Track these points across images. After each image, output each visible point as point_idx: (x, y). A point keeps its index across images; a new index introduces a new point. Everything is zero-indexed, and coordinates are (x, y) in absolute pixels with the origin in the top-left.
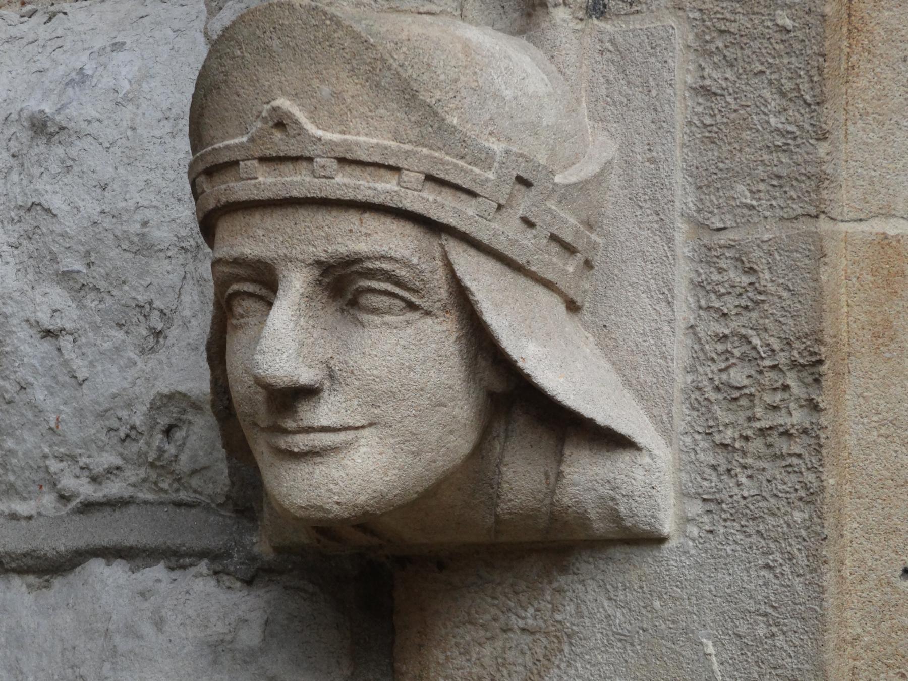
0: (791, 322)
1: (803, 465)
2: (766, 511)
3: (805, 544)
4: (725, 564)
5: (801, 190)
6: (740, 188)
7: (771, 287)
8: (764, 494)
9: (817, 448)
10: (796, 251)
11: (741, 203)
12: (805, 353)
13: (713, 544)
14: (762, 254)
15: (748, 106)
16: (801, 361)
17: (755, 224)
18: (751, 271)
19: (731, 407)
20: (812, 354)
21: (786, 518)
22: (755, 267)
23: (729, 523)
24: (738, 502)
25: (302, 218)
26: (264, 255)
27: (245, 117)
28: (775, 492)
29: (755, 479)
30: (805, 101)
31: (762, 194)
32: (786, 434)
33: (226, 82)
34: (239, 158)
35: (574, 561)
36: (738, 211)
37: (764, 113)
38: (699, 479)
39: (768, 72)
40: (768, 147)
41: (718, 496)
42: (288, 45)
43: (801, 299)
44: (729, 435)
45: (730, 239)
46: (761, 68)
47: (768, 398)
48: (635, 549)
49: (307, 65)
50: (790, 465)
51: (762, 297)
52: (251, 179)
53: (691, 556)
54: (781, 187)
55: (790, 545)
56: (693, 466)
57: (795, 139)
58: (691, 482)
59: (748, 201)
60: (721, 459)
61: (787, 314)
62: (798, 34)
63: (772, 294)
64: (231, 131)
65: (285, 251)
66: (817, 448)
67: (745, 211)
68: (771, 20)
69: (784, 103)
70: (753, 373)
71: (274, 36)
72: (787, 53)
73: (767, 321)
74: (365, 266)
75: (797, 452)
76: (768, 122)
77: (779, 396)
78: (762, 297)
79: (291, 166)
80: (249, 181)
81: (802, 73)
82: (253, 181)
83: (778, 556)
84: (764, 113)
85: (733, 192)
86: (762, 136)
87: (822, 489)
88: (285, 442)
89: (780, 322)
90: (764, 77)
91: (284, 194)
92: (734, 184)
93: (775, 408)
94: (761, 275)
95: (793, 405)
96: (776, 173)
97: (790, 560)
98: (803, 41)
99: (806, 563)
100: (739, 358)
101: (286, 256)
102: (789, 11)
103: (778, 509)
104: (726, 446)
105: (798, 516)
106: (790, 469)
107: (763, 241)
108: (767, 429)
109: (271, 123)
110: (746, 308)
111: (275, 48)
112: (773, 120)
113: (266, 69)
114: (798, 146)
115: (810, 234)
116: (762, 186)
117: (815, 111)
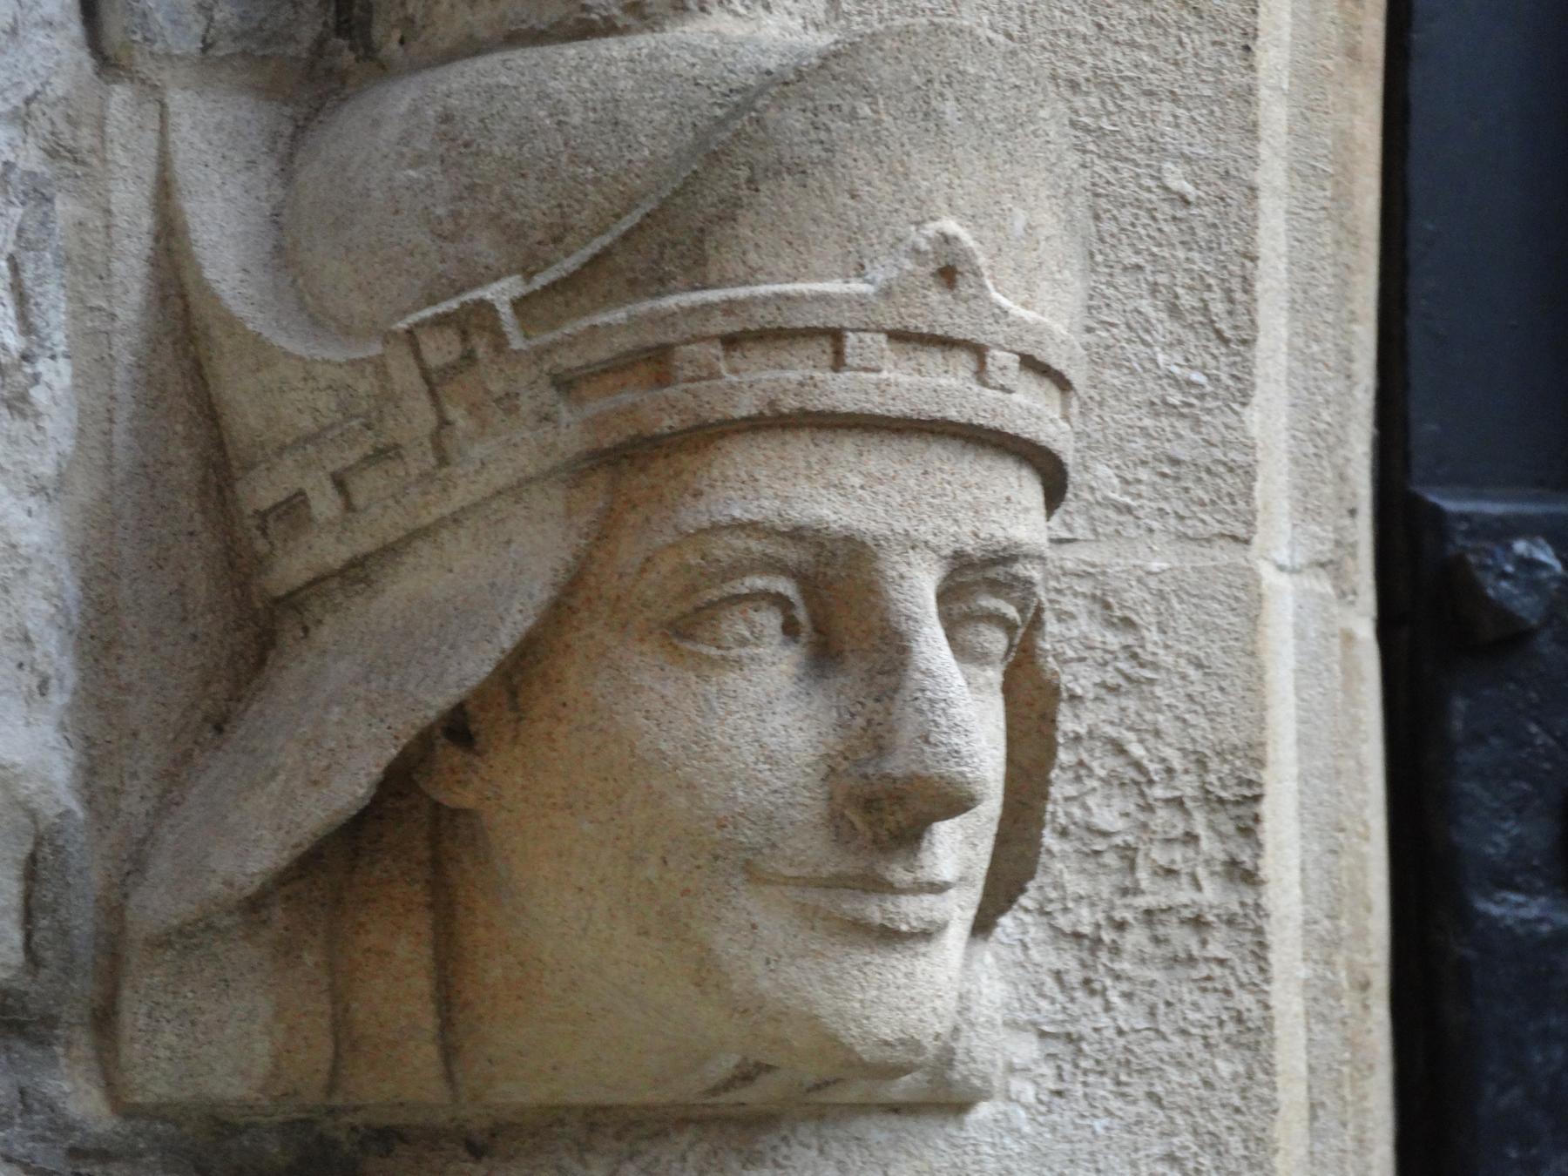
0: (1203, 722)
1: (1232, 980)
2: (1166, 1058)
3: (1239, 1117)
4: (1092, 1154)
5: (1218, 491)
6: (1102, 470)
7: (1166, 659)
8: (1163, 1028)
9: (1256, 949)
10: (1213, 598)
11: (1105, 498)
12: (1231, 782)
13: (1068, 1114)
14: (1148, 597)
15: (1113, 325)
16: (1223, 794)
17: (1130, 539)
18: (1128, 623)
19: (1087, 866)
20: (1242, 782)
21: (1202, 1070)
22: (1134, 617)
23: (1091, 1079)
24: (1111, 1041)
25: (938, 464)
26: (862, 528)
27: (863, 242)
28: (1182, 1024)
29: (1136, 1000)
30: (1218, 333)
31: (1143, 488)
32: (1198, 923)
33: (828, 163)
34: (847, 324)
35: (776, 1141)
36: (1097, 512)
37: (1144, 342)
38: (1033, 995)
39: (1149, 268)
40: (1153, 404)
41: (1070, 1028)
42: (972, 117)
43: (1223, 684)
44: (1084, 917)
45: (1085, 562)
46: (1135, 260)
47: (1160, 855)
48: (910, 1123)
49: (999, 161)
50: (1209, 978)
51: (1148, 673)
52: (866, 370)
53: (1023, 1137)
54: (1177, 479)
55: (1214, 1120)
56: (1021, 971)
57: (1202, 397)
58: (1019, 1000)
59: (1115, 496)
60: (1069, 961)
61: (1198, 708)
62: (1206, 211)
63: (1168, 671)
64: (817, 264)
65: (906, 525)
66: (1256, 949)
67: (1112, 514)
68: (1152, 177)
69: (1176, 328)
70: (1132, 808)
71: (948, 92)
72: (1182, 243)
73: (1161, 718)
74: (1013, 571)
75: (1221, 955)
76: (1154, 361)
77: (1178, 854)
78: (1148, 673)
79: (939, 357)
80: (863, 375)
81: (1212, 281)
82: (873, 376)
83: (1187, 1138)
84: (1144, 342)
85: (1088, 476)
86: (1142, 383)
87: (1268, 1022)
88: (884, 911)
89: (1184, 721)
90: (1141, 277)
91: (932, 410)
92: (1089, 463)
93: (1170, 872)
94: (1145, 633)
95: (1201, 872)
96: (1171, 453)
97: (1212, 1146)
98: (1215, 226)
99: (1243, 1152)
100: (1101, 779)
101: (907, 533)
102: (1188, 168)
103: (1190, 1055)
104: (1078, 936)
105: (1224, 1068)
106: (1209, 985)
107: (1149, 573)
108: (1163, 911)
109: (932, 267)
110: (1114, 690)
111: (948, 118)
112: (1161, 358)
113: (926, 156)
114: (1209, 411)
115: (1234, 569)
116: (1144, 474)
117: (1238, 354)
